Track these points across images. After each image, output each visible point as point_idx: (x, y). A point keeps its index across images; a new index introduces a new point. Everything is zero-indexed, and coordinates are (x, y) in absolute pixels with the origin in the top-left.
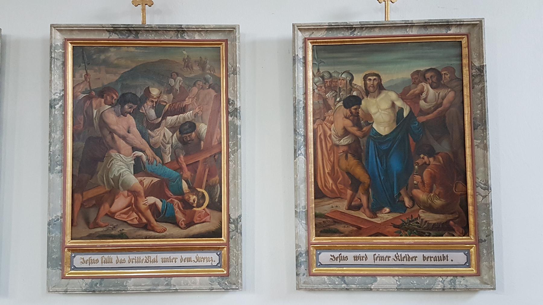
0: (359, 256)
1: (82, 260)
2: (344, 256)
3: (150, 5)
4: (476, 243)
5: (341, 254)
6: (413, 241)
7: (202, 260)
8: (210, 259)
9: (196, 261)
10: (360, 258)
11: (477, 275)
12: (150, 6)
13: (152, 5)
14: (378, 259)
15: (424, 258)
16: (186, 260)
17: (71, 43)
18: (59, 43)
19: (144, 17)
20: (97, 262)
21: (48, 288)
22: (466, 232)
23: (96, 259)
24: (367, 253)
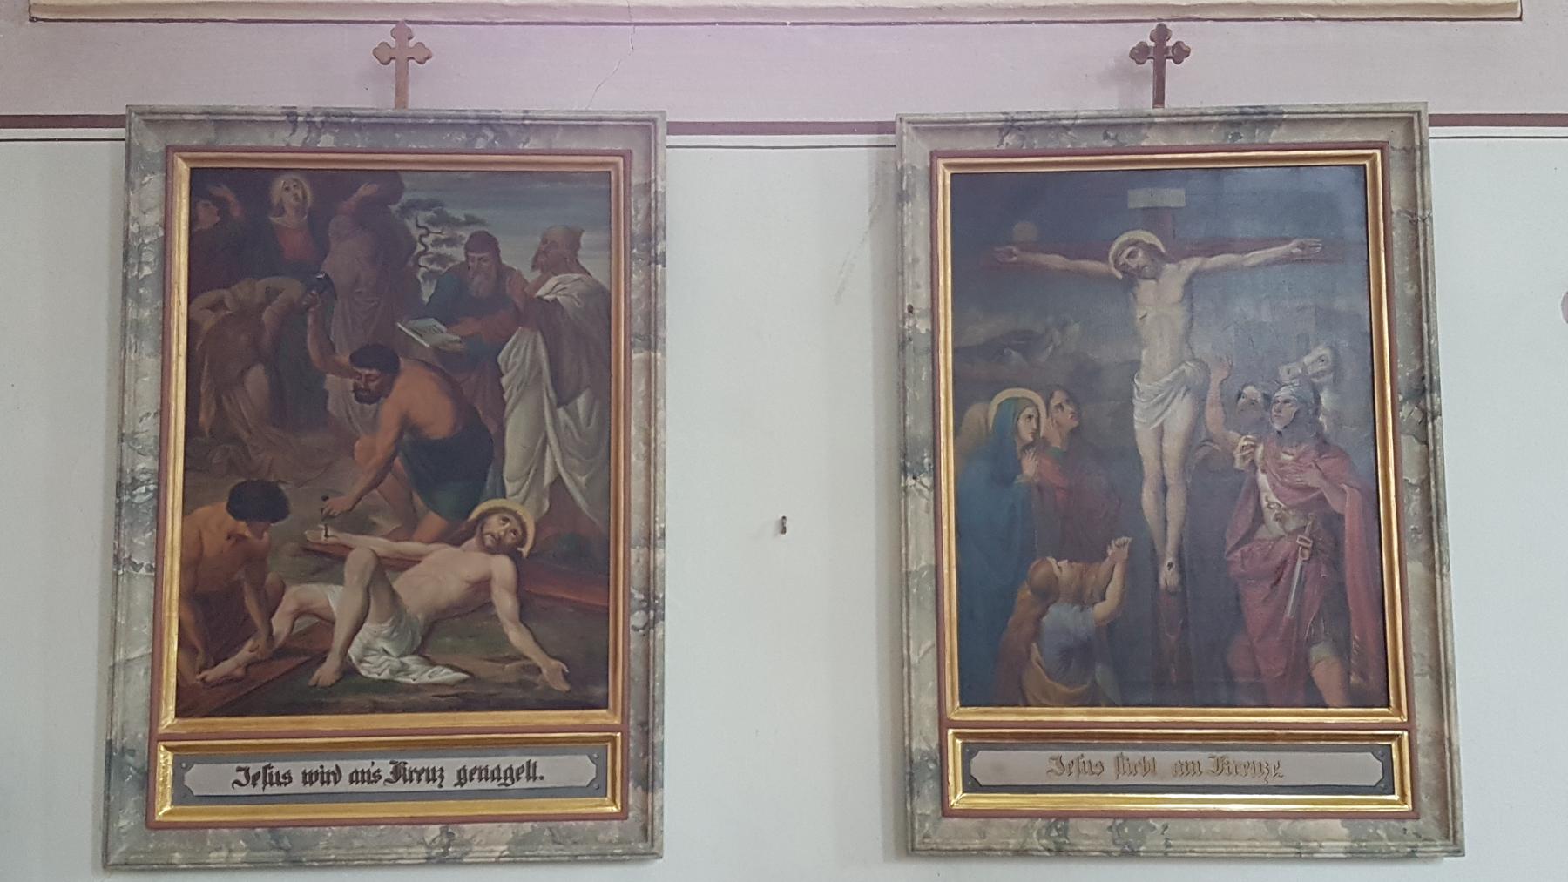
0: (320, 770)
1: (241, 777)
2: (278, 773)
3: (421, 58)
4: (1408, 726)
5: (269, 767)
6: (193, 728)
7: (415, 776)
8: (438, 774)
9: (244, 782)
10: (323, 777)
11: (1412, 814)
12: (420, 63)
13: (428, 58)
14: (476, 776)
15: (398, 773)
16: (476, 776)
17: (185, 160)
18: (922, 164)
19: (401, 92)
20: (287, 781)
21: (106, 853)
22: (962, 706)
23: (285, 771)
24: (339, 763)
